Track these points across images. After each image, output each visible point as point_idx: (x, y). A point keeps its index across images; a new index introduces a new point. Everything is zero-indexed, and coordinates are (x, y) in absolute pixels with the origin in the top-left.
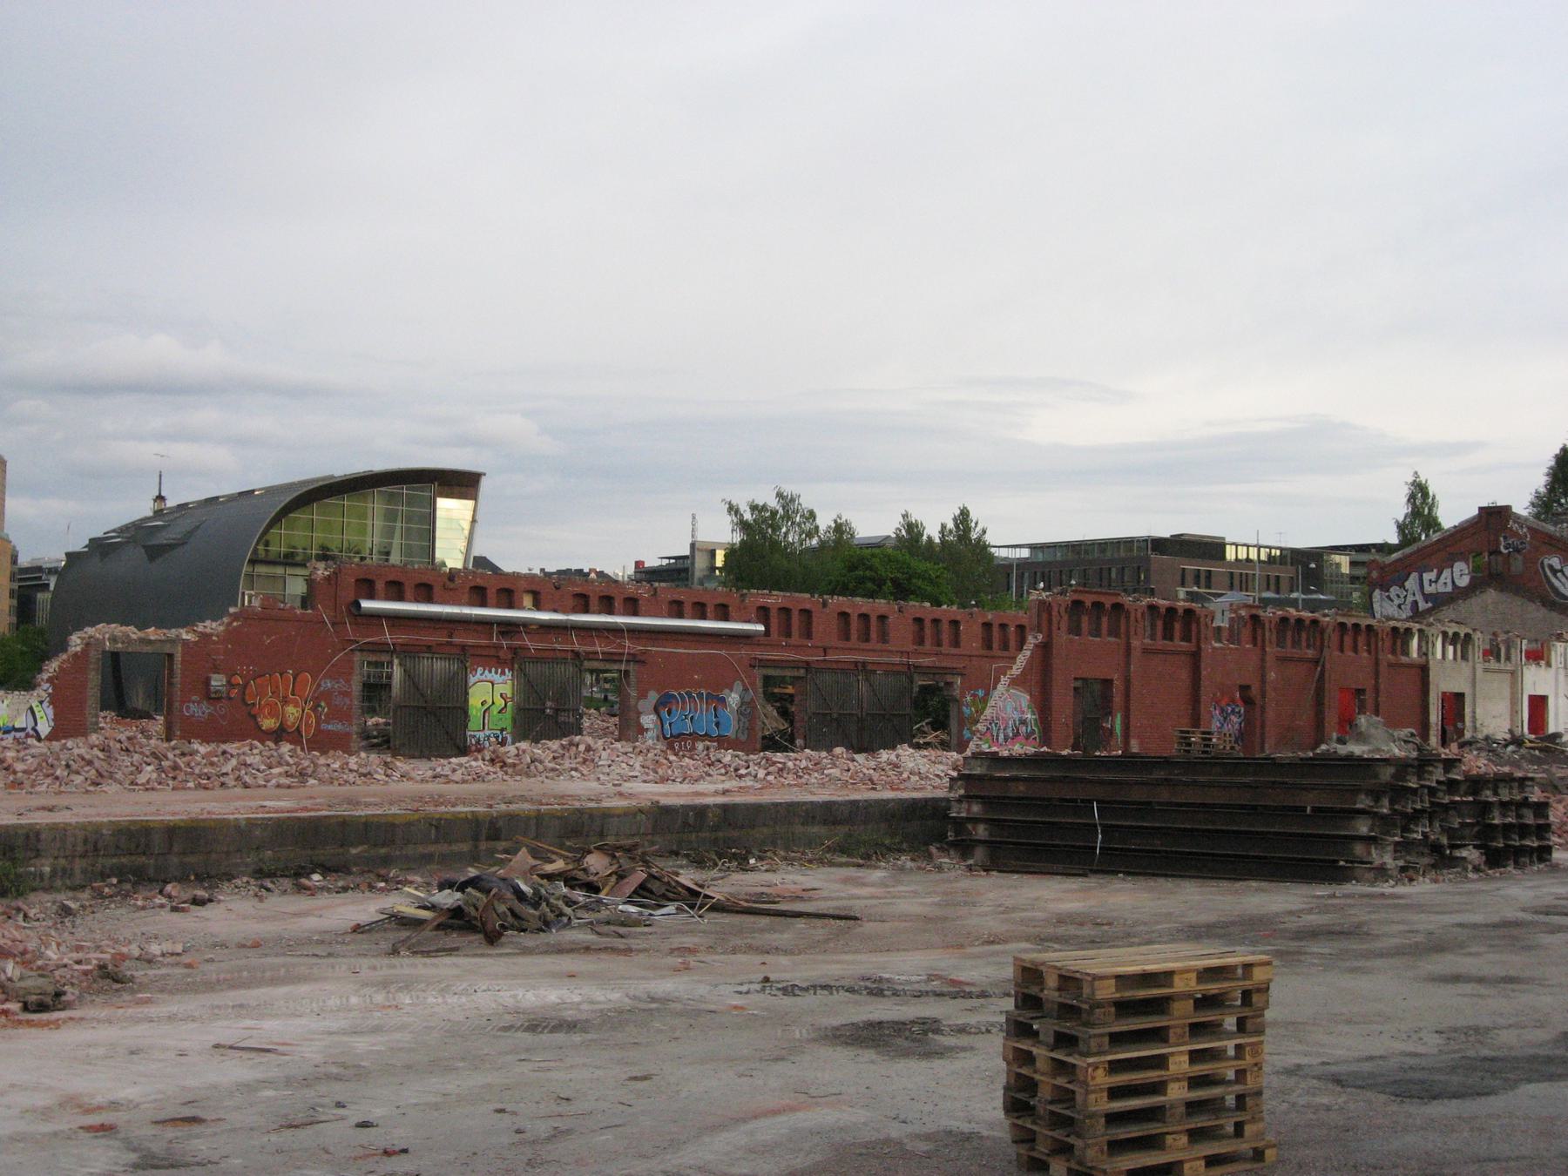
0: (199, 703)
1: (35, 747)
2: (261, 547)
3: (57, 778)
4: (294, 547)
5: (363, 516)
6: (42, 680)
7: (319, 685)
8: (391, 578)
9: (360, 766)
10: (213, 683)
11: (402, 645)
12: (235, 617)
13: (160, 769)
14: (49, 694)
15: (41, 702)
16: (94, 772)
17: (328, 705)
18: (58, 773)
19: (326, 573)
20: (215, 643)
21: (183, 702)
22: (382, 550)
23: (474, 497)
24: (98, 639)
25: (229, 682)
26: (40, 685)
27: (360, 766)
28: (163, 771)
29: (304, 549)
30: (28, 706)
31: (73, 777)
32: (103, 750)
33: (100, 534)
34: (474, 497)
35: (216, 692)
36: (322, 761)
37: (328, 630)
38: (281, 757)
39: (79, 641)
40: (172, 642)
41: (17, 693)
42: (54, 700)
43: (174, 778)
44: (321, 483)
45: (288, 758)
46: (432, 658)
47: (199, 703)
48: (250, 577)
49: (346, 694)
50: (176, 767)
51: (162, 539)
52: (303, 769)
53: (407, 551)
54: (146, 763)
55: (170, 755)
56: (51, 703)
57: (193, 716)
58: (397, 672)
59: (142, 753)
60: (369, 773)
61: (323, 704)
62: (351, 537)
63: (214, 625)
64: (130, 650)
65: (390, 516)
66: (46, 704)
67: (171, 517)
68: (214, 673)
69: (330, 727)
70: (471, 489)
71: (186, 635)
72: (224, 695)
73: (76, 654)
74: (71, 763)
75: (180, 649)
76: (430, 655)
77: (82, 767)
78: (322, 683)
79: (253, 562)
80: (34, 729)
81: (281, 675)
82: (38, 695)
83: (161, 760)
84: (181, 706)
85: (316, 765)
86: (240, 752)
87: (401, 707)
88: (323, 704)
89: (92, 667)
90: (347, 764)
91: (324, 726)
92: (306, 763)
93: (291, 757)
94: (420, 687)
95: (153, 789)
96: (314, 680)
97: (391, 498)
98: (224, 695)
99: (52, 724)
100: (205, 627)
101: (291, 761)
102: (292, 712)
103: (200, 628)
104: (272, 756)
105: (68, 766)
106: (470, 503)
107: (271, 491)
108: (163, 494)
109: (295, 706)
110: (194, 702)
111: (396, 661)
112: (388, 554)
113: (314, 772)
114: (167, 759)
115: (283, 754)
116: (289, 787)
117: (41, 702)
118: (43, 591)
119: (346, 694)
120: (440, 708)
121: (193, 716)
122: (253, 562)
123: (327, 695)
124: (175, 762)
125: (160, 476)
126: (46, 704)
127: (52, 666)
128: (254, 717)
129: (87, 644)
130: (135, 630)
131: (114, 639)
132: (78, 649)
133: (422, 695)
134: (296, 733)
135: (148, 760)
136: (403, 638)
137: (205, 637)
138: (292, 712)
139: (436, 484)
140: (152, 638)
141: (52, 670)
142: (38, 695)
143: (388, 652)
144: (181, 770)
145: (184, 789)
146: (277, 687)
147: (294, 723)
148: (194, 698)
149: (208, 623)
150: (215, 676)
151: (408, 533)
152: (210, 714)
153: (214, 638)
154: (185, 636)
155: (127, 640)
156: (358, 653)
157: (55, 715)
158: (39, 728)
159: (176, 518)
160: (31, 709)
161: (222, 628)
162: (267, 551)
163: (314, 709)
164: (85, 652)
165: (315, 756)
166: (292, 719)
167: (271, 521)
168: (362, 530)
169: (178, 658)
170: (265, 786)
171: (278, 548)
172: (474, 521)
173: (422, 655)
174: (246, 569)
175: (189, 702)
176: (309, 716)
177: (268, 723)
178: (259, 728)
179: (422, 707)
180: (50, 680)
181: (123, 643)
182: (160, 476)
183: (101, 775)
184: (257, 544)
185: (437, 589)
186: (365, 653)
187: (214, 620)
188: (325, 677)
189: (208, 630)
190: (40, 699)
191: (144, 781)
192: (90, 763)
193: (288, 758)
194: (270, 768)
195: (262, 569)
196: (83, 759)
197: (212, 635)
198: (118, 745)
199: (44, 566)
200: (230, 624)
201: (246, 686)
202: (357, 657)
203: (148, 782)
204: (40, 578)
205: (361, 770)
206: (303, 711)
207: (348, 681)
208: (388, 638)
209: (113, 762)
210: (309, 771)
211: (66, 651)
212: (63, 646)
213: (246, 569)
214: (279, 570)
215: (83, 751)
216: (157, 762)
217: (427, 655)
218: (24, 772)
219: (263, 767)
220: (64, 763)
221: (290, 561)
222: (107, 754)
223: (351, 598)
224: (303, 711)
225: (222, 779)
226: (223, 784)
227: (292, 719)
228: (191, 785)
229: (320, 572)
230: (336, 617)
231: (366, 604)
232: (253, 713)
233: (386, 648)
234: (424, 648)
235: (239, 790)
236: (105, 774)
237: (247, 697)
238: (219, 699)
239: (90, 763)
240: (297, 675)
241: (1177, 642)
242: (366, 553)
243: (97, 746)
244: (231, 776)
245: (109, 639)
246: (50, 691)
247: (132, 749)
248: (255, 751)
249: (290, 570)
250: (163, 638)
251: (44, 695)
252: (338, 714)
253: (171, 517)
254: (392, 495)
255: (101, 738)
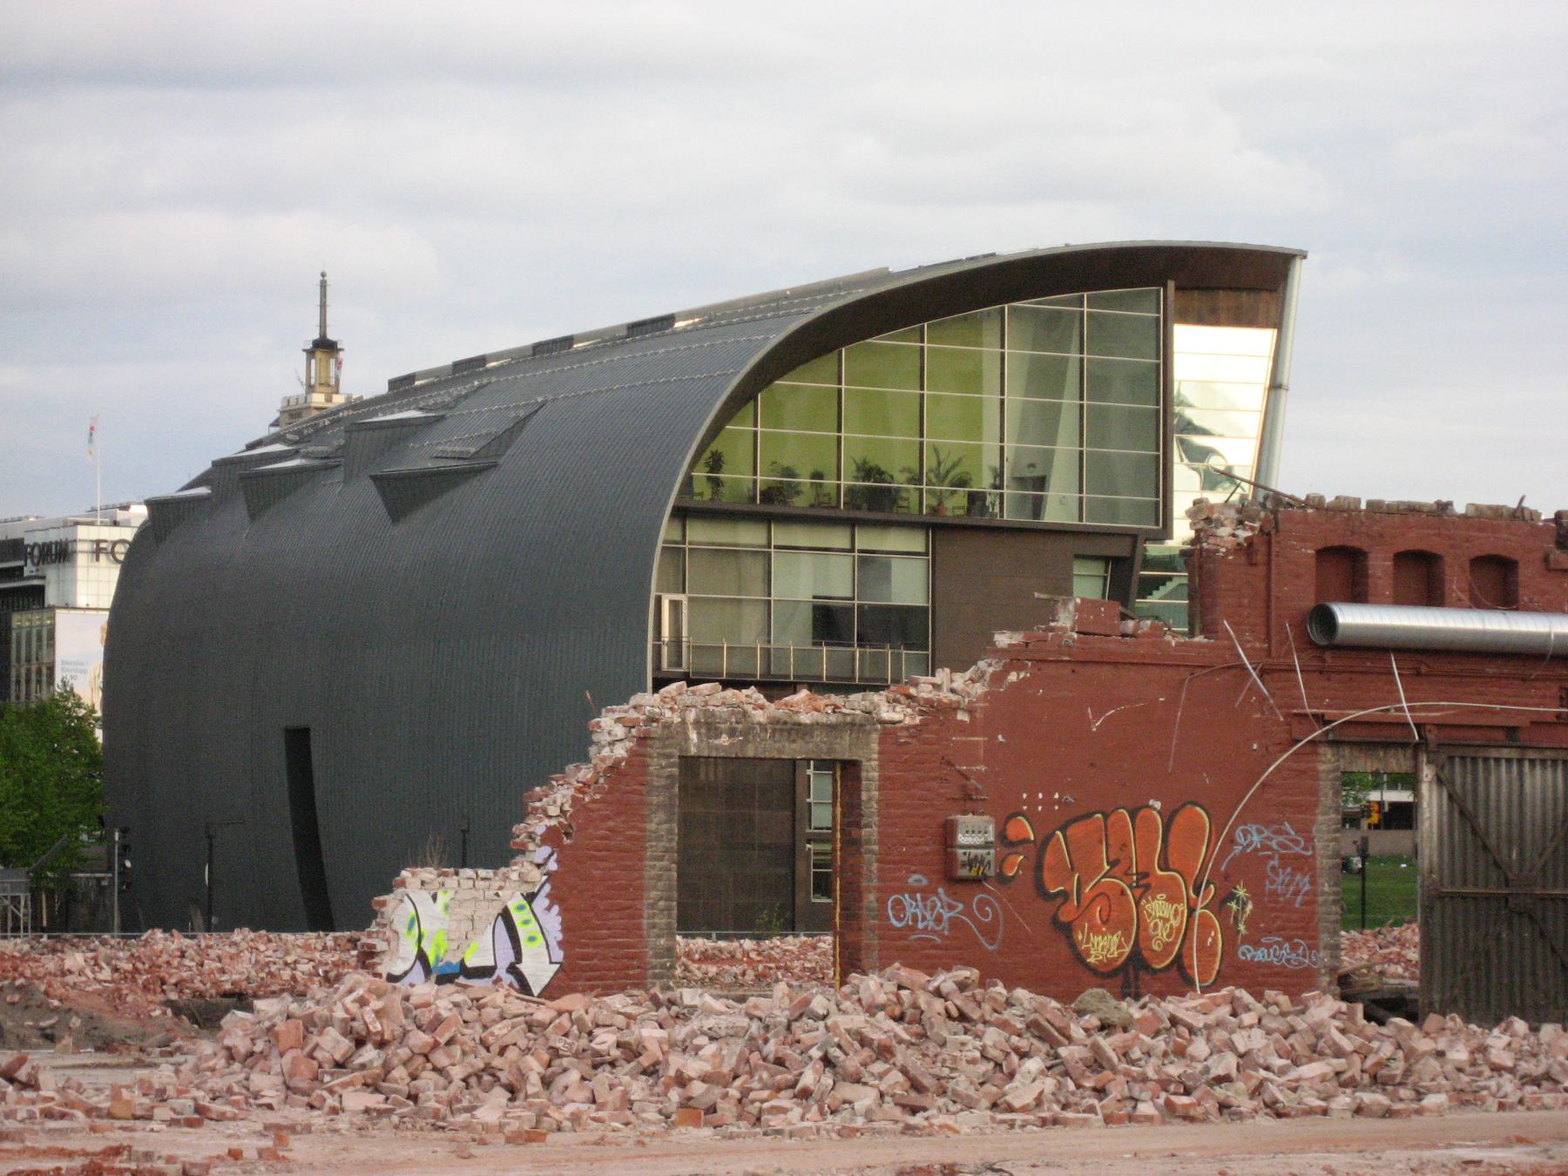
0: (927, 892)
1: (709, 1012)
2: (700, 474)
3: (805, 1094)
4: (789, 472)
5: (973, 380)
6: (531, 836)
7: (1231, 841)
8: (1411, 542)
9: (1520, 1055)
10: (962, 839)
11: (1439, 726)
12: (1014, 658)
13: (1055, 1065)
14: (549, 874)
15: (530, 898)
16: (896, 1076)
17: (1256, 896)
18: (808, 1079)
19: (1243, 534)
20: (962, 728)
21: (884, 893)
22: (1028, 473)
23: (1276, 321)
24: (667, 726)
25: (1002, 836)
26: (522, 851)
27: (1520, 1055)
28: (1066, 1074)
29: (817, 475)
30: (498, 909)
31: (847, 1090)
32: (899, 1019)
33: (232, 447)
34: (1276, 321)
35: (970, 863)
36: (1423, 1045)
37: (1254, 689)
38: (1317, 1032)
39: (620, 731)
40: (857, 727)
41: (468, 872)
42: (562, 891)
43: (1100, 1092)
44: (860, 294)
45: (1337, 1036)
46: (1520, 761)
47: (927, 892)
48: (675, 552)
49: (1300, 864)
50: (1097, 1063)
51: (420, 458)
52: (1381, 1064)
53: (1090, 472)
54: (1017, 1050)
55: (1077, 1032)
56: (554, 898)
57: (913, 929)
58: (1431, 803)
59: (1004, 1025)
60: (1547, 1076)
61: (1241, 892)
62: (945, 441)
63: (959, 680)
64: (750, 753)
65: (1046, 378)
66: (541, 902)
67: (444, 396)
68: (965, 812)
69: (1260, 955)
70: (1265, 296)
71: (889, 711)
72: (991, 872)
73: (615, 767)
74: (835, 1052)
75: (875, 746)
76: (1514, 754)
77: (865, 1065)
78: (1239, 833)
79: (682, 514)
80: (513, 969)
81: (1133, 816)
82: (523, 880)
83: (1054, 1044)
84: (882, 902)
85: (1411, 1055)
86: (1211, 1019)
87: (1442, 897)
88: (1241, 892)
89: (655, 800)
90: (1483, 1049)
91: (1246, 953)
92: (1387, 1049)
93: (1343, 1031)
94: (1492, 840)
95: (1055, 1121)
96: (1217, 829)
97: (1051, 329)
98: (991, 872)
99: (559, 955)
100: (937, 687)
101: (1346, 1043)
102: (1163, 915)
103: (924, 690)
104: (1293, 1031)
105: (827, 1061)
106: (1264, 338)
107: (716, 319)
108: (331, 336)
109: (1172, 899)
110: (912, 892)
111: (1427, 773)
112: (1041, 483)
113: (1408, 1072)
114: (1069, 1038)
115: (1321, 1024)
116: (1389, 1113)
117: (530, 898)
118: (26, 608)
119: (1300, 864)
120: (1543, 899)
121: (913, 929)
122: (682, 514)
123: (1250, 867)
124: (1096, 1048)
125: (323, 285)
126: (541, 902)
127: (557, 799)
128: (1066, 930)
129: (643, 740)
130: (761, 699)
131: (708, 725)
132: (620, 751)
133: (1497, 864)
134: (1174, 973)
135: (1023, 1044)
136: (1442, 707)
137: (937, 713)
138: (1163, 915)
139: (1171, 284)
140: (805, 718)
141: (554, 811)
142: (523, 880)
143: (1404, 745)
144: (1114, 1070)
145: (1131, 1118)
146: (1124, 846)
147: (1167, 947)
148: (913, 879)
149: (942, 675)
150: (966, 820)
151: (1093, 426)
152: (955, 924)
153: (962, 716)
154: (886, 714)
155: (742, 726)
156: (1327, 753)
157: (565, 929)
158: (523, 967)
159: (459, 399)
160: (506, 915)
161: (979, 689)
162: (716, 483)
163: (1220, 904)
164: (637, 758)
165: (1400, 1029)
166: (1162, 934)
167: (726, 403)
168: (973, 426)
169: (871, 772)
170: (1325, 1112)
171: (740, 477)
172: (1275, 386)
173: (1493, 753)
174: (666, 531)
175: (900, 891)
176: (1206, 926)
177: (1103, 947)
178: (1079, 958)
179: (1497, 897)
180: (551, 837)
181: (732, 733)
182: (323, 285)
183: (917, 1087)
184: (692, 466)
185: (1527, 573)
186: (1347, 751)
187: (960, 667)
188: (1241, 820)
189: (945, 696)
190: (528, 889)
191: (1029, 1098)
192: (884, 1052)
193: (1337, 1036)
194: (1296, 1063)
195: (699, 533)
196: (864, 1041)
197: (954, 708)
198: (939, 1005)
199: (29, 540)
200: (998, 678)
201: (1045, 842)
202: (1327, 762)
203: (1039, 1102)
204: (16, 573)
205: (1527, 1067)
206: (1191, 910)
207: (1305, 830)
208: (1404, 707)
209: (932, 1048)
210: (1398, 1068)
211: (586, 759)
212: (579, 746)
213: (666, 531)
214: (749, 536)
215: (858, 1020)
216: (1045, 1048)
217: (1506, 753)
218: (705, 1079)
219: (1278, 1062)
220: (816, 1053)
221: (776, 508)
222: (916, 1028)
223: (1309, 603)
224: (1191, 910)
225: (1220, 1092)
226: (1223, 1107)
227: (1162, 934)
228: (1145, 1108)
229: (1225, 532)
230: (1269, 653)
231: (1350, 617)
232: (1063, 918)
233: (1397, 735)
234: (1500, 736)
235: (1266, 1122)
236: (927, 1081)
237: (1047, 876)
238: (977, 881)
239: (884, 1052)
240: (1175, 813)
241: (813, 870)
242: (984, 483)
243: (882, 1007)
244: (1240, 1085)
245: (697, 723)
246: (553, 866)
247: (975, 1015)
248: (1248, 1018)
249: (780, 535)
250: (833, 719)
251: (537, 876)
252: (1301, 927)
253: (444, 396)
254: (1053, 320)
255: (891, 987)
